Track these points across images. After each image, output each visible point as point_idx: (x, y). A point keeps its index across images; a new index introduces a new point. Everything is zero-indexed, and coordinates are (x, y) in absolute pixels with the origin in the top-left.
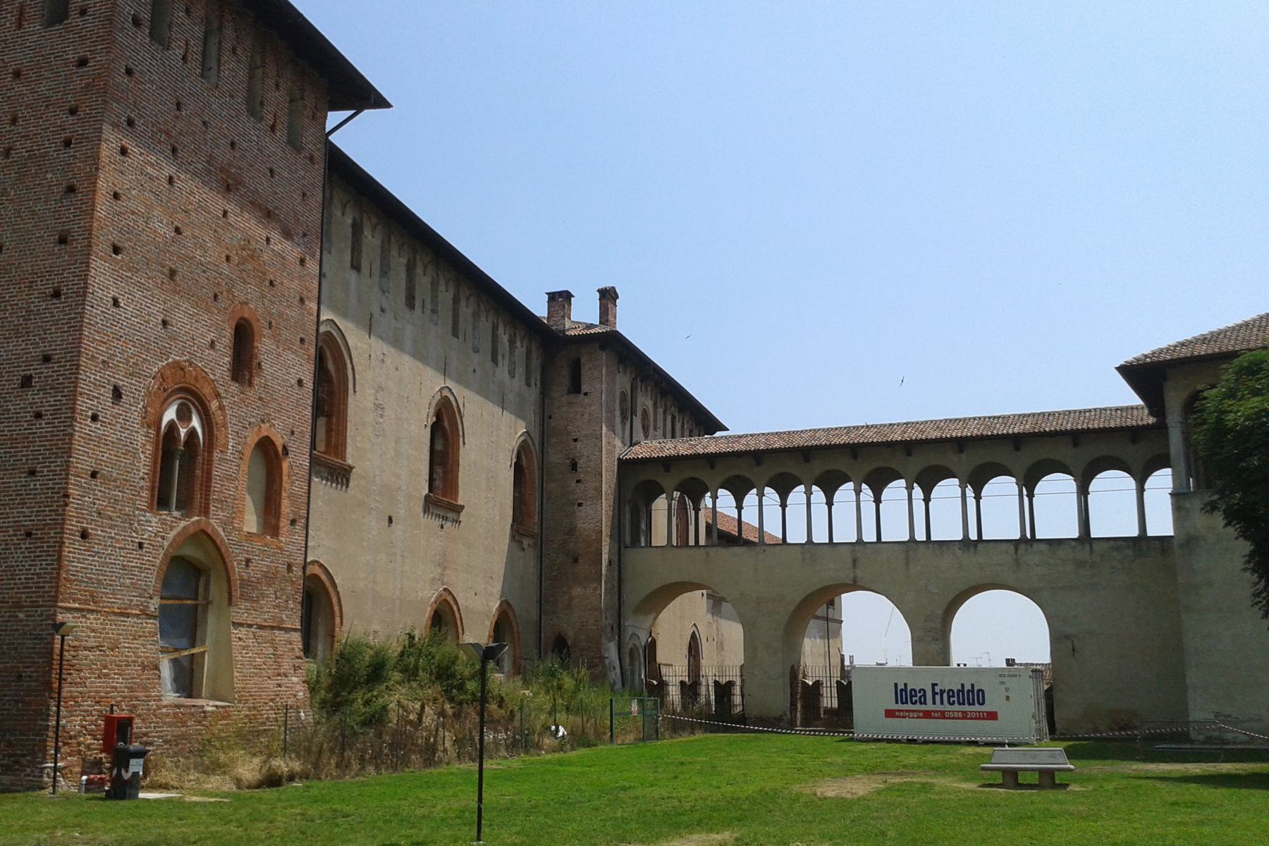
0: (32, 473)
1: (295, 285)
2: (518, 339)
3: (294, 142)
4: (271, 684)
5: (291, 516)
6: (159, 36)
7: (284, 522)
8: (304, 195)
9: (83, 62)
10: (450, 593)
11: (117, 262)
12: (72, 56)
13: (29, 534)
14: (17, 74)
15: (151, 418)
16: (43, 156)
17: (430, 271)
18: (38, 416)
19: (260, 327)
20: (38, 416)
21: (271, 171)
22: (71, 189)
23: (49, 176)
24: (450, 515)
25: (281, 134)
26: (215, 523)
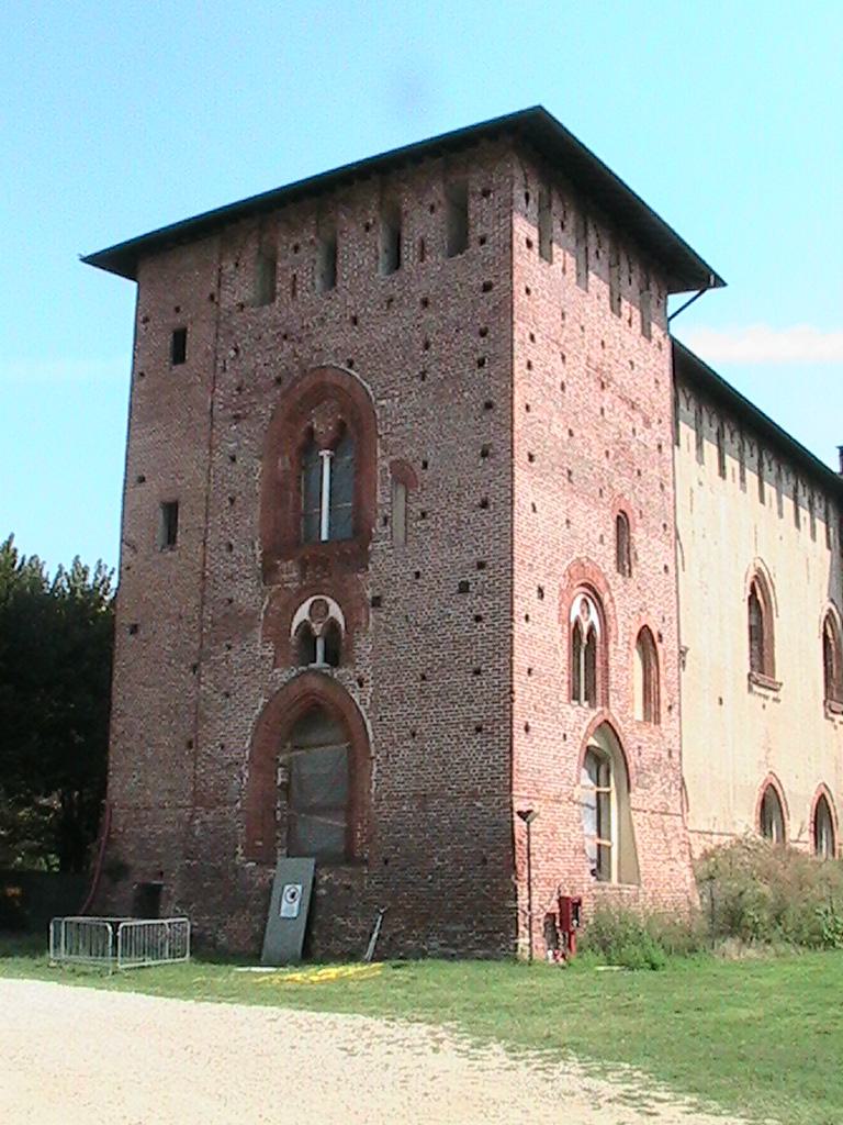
0: (477, 672)
1: (656, 472)
2: (816, 499)
3: (646, 333)
4: (666, 868)
5: (668, 703)
6: (546, 256)
7: (663, 709)
8: (657, 381)
9: (487, 287)
10: (774, 775)
11: (533, 469)
12: (477, 282)
13: (479, 729)
14: (425, 303)
15: (564, 617)
16: (459, 376)
17: (737, 438)
18: (478, 619)
19: (634, 517)
20: (478, 619)
21: (632, 363)
22: (489, 406)
23: (466, 394)
24: (771, 694)
25: (637, 327)
26: (614, 714)
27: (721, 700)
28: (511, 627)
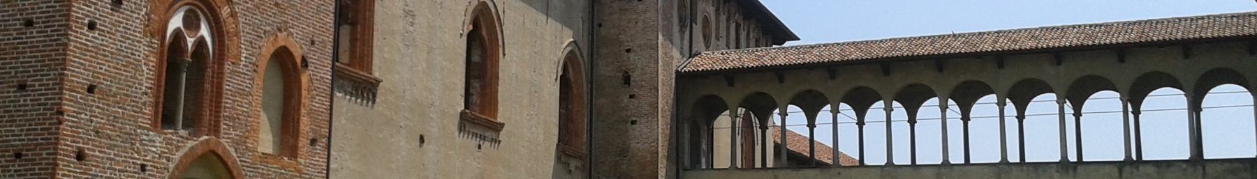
0: (22, 87)
5: (311, 135)
7: (303, 142)
13: (18, 156)
18: (29, 23)
20: (29, 23)
24: (489, 134)
26: (226, 143)
27: (422, 139)
28: (66, 35)
